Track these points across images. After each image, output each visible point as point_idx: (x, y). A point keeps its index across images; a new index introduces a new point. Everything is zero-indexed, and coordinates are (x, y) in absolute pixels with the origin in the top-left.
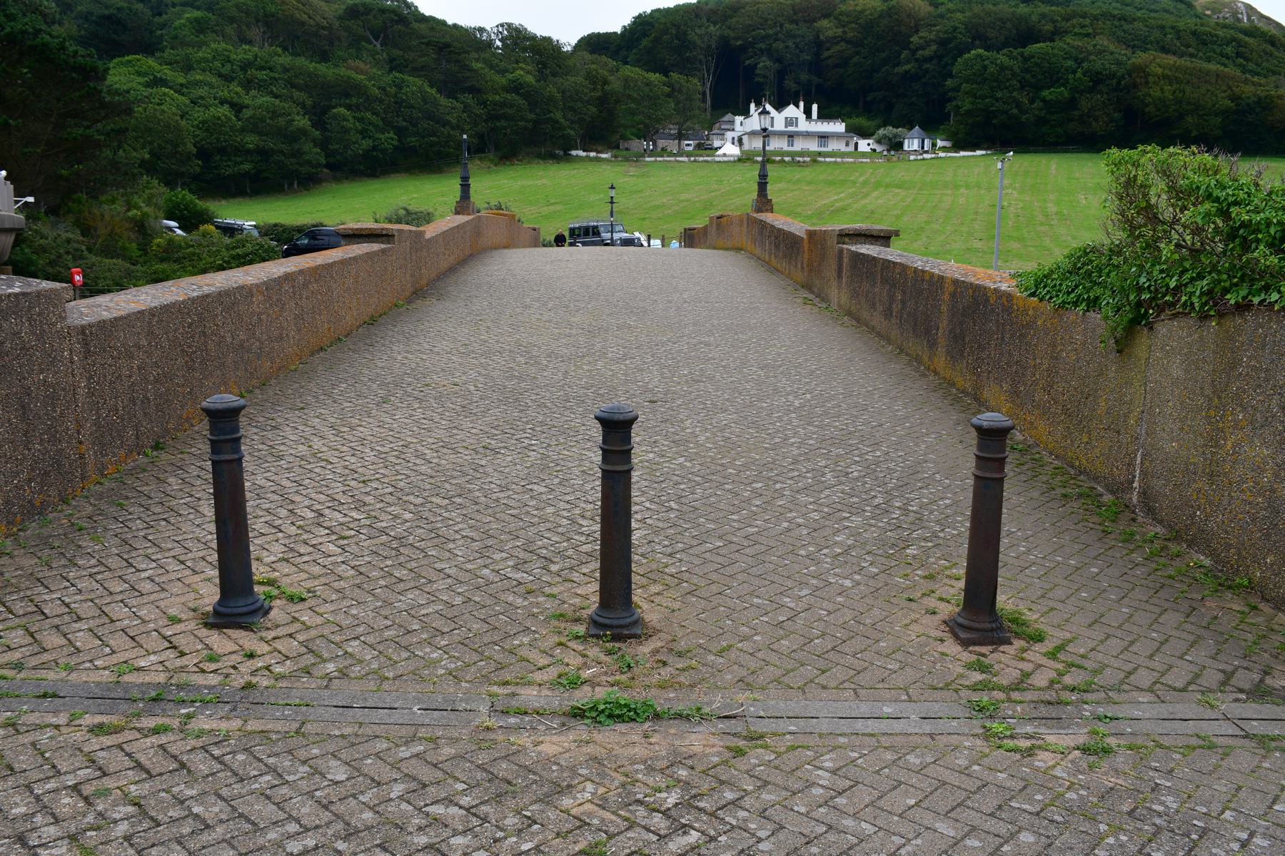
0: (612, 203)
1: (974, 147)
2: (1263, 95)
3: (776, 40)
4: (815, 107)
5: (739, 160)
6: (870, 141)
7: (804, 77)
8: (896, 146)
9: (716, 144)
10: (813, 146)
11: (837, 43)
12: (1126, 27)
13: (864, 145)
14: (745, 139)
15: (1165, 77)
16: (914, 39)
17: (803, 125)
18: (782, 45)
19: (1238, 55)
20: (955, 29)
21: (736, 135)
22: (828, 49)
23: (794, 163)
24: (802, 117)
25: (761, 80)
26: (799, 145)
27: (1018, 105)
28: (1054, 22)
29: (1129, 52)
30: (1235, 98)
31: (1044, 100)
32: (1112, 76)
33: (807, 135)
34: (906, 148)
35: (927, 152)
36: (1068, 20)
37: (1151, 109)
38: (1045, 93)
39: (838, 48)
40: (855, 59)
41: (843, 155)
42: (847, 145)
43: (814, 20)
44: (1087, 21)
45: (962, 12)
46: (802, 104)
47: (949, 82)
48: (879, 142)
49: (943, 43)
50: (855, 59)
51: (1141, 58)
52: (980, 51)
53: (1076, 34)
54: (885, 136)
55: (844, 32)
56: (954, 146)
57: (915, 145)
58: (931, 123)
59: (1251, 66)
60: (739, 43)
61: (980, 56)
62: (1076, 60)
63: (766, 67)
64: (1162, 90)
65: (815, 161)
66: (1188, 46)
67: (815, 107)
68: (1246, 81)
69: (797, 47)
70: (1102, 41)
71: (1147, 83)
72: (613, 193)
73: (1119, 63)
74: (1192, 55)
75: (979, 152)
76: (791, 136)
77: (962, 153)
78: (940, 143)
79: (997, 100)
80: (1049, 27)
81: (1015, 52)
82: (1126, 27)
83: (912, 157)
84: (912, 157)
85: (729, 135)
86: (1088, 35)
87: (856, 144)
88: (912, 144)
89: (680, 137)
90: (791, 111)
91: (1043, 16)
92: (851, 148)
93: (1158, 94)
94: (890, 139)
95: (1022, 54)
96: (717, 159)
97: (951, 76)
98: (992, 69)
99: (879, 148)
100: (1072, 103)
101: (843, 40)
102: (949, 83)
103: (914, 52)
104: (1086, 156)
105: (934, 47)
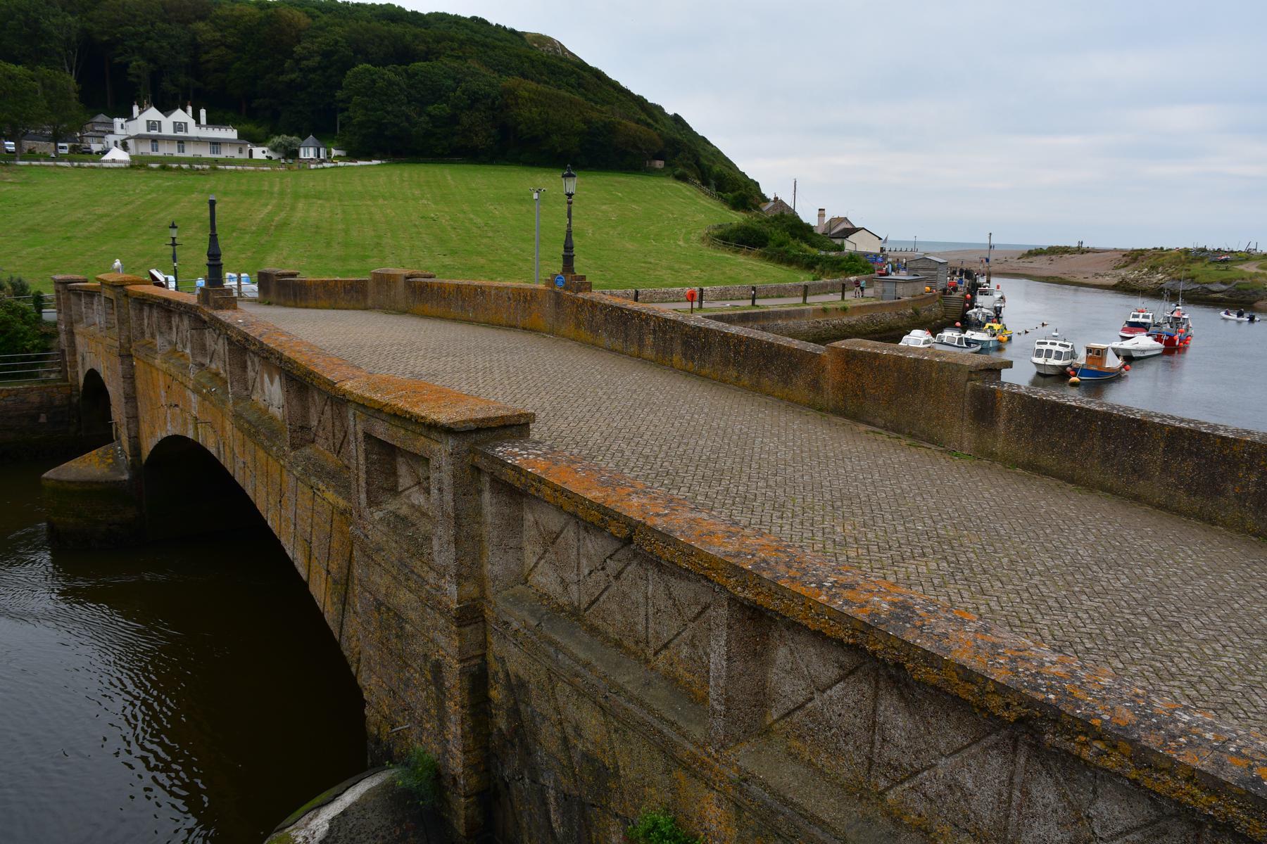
0: (174, 244)
1: (369, 157)
2: (607, 120)
3: (148, 39)
4: (203, 112)
5: (132, 167)
6: (265, 149)
7: (183, 79)
8: (292, 154)
9: (96, 147)
10: (206, 153)
11: (217, 47)
12: (490, 53)
13: (259, 153)
14: (131, 143)
15: (532, 100)
16: (297, 49)
17: (193, 131)
18: (155, 45)
19: (580, 85)
20: (337, 42)
21: (119, 139)
22: (207, 53)
23: (192, 171)
24: (191, 122)
25: (135, 80)
26: (190, 152)
27: (408, 118)
28: (426, 42)
29: (496, 75)
30: (587, 122)
31: (429, 115)
32: (487, 96)
33: (199, 141)
34: (302, 156)
35: (323, 161)
36: (439, 42)
37: (522, 127)
38: (430, 108)
39: (217, 52)
40: (237, 65)
41: (240, 162)
42: (240, 151)
43: (189, 22)
44: (456, 45)
45: (340, 25)
46: (190, 109)
47: (339, 94)
48: (274, 150)
49: (326, 55)
50: (237, 65)
51: (509, 82)
52: (369, 66)
53: (449, 56)
54: (280, 145)
55: (224, 36)
56: (348, 155)
57: (311, 153)
58: (324, 131)
59: (591, 96)
60: (106, 38)
61: (368, 70)
62: (454, 79)
63: (139, 67)
64: (530, 111)
65: (216, 169)
66: (542, 74)
67: (203, 112)
68: (592, 109)
69: (172, 47)
70: (474, 64)
71: (517, 104)
72: (174, 233)
73: (491, 85)
74: (546, 82)
75: (375, 162)
76: (181, 142)
77: (360, 163)
78: (334, 152)
79: (388, 113)
80: (422, 47)
81: (400, 69)
82: (490, 53)
83: (313, 166)
84: (313, 166)
85: (110, 139)
86: (459, 58)
87: (251, 152)
88: (307, 153)
89: (56, 138)
90: (179, 115)
91: (416, 36)
92: (245, 156)
93: (527, 114)
94: (286, 148)
95: (406, 71)
96: (105, 165)
97: (341, 89)
98: (380, 84)
99: (275, 157)
100: (453, 119)
101: (223, 44)
102: (339, 94)
103: (298, 61)
104: (472, 167)
105: (318, 59)
